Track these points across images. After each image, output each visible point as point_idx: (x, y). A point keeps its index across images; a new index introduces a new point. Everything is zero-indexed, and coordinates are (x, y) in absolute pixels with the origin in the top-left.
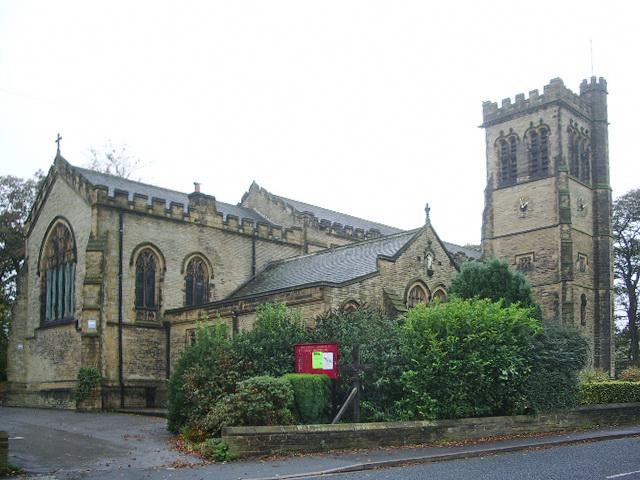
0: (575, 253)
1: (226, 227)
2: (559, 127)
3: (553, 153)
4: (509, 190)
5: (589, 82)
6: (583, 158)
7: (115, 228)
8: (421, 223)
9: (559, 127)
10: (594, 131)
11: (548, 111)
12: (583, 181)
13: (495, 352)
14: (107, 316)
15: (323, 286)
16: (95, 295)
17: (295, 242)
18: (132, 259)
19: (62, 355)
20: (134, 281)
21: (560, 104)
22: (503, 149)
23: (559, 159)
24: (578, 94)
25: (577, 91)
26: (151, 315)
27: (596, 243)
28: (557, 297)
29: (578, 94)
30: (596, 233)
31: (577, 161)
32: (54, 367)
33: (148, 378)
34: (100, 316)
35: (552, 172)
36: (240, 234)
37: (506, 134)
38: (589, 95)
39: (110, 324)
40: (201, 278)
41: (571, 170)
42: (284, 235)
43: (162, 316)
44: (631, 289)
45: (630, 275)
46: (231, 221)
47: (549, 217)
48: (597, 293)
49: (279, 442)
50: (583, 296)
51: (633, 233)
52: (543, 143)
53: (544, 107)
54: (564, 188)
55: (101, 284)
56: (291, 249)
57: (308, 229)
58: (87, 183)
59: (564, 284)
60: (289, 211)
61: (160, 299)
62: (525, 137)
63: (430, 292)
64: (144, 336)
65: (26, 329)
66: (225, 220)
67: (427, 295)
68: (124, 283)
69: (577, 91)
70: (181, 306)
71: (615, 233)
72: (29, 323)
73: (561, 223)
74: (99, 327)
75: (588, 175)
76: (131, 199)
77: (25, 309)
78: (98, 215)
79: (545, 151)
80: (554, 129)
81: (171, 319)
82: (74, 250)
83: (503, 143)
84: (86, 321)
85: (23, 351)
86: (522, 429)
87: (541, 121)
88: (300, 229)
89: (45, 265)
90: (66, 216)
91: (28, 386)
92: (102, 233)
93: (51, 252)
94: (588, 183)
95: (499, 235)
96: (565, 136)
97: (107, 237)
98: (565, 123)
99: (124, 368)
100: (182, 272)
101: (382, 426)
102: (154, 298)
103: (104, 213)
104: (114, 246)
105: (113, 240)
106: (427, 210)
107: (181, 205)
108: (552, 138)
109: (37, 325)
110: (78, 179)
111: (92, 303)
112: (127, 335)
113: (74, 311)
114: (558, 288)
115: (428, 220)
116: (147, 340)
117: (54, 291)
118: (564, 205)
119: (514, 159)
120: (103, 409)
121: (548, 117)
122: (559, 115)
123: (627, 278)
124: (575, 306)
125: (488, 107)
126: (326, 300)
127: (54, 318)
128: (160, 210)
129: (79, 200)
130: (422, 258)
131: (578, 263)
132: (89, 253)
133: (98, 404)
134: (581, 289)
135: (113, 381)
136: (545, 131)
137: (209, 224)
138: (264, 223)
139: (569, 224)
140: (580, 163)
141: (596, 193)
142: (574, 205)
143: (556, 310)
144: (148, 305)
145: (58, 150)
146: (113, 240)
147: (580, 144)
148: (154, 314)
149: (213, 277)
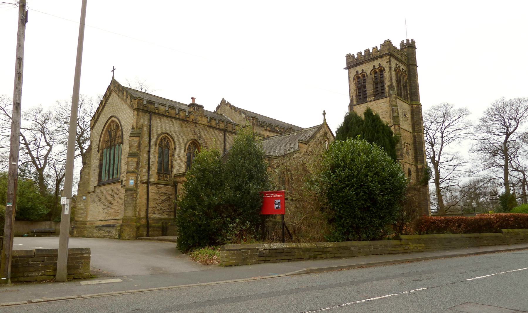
0: (403, 143)
1: (209, 124)
2: (390, 68)
3: (387, 83)
5: (405, 42)
6: (404, 87)
7: (147, 123)
8: (321, 122)
9: (390, 68)
10: (409, 71)
11: (384, 59)
12: (405, 99)
14: (141, 178)
16: (134, 164)
19: (111, 203)
20: (157, 155)
21: (391, 55)
23: (391, 87)
24: (399, 49)
25: (398, 47)
26: (166, 177)
27: (414, 137)
29: (399, 49)
30: (413, 133)
31: (401, 88)
32: (106, 210)
33: (164, 217)
34: (137, 177)
35: (387, 95)
37: (377, 67)
38: (405, 50)
39: (142, 182)
43: (173, 178)
50: (409, 169)
53: (381, 57)
60: (243, 116)
61: (172, 167)
62: (371, 74)
64: (162, 190)
65: (88, 186)
66: (209, 120)
68: (151, 157)
69: (398, 47)
72: (91, 183)
74: (136, 184)
75: (407, 96)
76: (156, 105)
77: (89, 174)
78: (138, 115)
79: (382, 82)
80: (387, 69)
83: (358, 78)
85: (86, 201)
87: (380, 65)
89: (102, 146)
91: (88, 223)
93: (107, 138)
94: (408, 101)
96: (394, 73)
98: (393, 66)
99: (150, 210)
100: (185, 151)
102: (168, 166)
103: (140, 114)
104: (146, 135)
106: (324, 114)
107: (184, 111)
108: (386, 74)
109: (96, 184)
110: (125, 93)
115: (325, 120)
116: (164, 193)
117: (108, 162)
118: (395, 114)
119: (365, 87)
121: (384, 62)
122: (390, 61)
127: (107, 179)
128: (172, 112)
129: (126, 106)
131: (405, 149)
134: (408, 165)
136: (382, 71)
138: (229, 122)
139: (399, 125)
140: (403, 89)
141: (412, 107)
142: (400, 114)
144: (165, 171)
145: (113, 77)
146: (146, 131)
148: (168, 176)
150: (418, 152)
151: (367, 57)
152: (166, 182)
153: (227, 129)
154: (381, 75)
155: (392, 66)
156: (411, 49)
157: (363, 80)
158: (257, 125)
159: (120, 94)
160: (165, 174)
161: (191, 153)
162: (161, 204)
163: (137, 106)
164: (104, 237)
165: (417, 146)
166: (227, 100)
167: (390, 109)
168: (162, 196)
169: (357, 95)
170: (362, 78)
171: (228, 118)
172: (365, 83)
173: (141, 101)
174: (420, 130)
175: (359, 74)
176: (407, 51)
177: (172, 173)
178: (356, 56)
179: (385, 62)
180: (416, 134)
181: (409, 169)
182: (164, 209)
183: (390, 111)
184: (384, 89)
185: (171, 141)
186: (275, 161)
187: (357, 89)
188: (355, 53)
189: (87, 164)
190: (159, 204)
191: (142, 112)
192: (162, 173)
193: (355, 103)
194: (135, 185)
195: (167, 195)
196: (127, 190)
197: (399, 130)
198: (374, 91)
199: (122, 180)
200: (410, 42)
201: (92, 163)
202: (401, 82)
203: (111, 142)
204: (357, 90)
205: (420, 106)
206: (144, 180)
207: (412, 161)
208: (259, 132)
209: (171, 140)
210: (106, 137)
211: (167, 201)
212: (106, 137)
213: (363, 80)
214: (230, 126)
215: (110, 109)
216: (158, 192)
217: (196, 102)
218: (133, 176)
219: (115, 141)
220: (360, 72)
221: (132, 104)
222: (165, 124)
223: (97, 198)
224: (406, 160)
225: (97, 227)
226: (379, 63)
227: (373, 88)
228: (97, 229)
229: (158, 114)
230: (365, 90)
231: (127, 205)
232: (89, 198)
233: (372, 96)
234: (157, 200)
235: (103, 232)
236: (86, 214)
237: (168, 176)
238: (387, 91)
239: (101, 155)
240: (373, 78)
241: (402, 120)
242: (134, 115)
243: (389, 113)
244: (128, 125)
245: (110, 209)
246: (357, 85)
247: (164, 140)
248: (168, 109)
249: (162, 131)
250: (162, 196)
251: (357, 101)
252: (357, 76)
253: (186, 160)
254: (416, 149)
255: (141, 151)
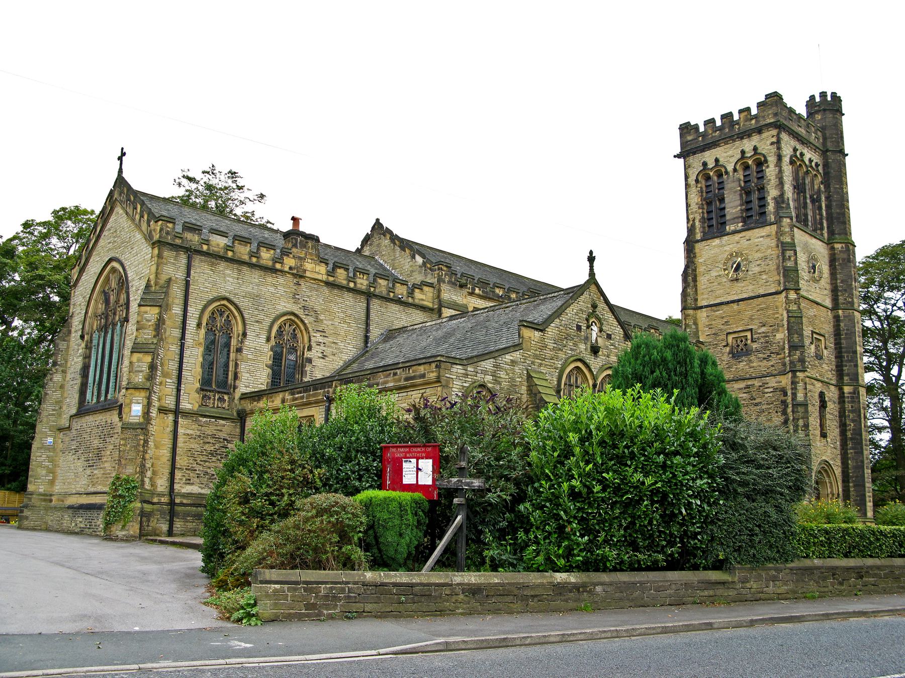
0: (807, 332)
1: (331, 279)
2: (780, 158)
3: (772, 193)
4: (717, 242)
7: (180, 275)
9: (780, 158)
11: (765, 135)
12: (815, 232)
13: (664, 466)
14: (159, 400)
15: (439, 362)
16: (145, 368)
17: (426, 303)
18: (200, 318)
20: (201, 349)
22: (707, 186)
23: (780, 200)
25: (802, 110)
26: (221, 400)
27: (837, 318)
28: (785, 394)
30: (836, 306)
31: (805, 204)
32: (88, 472)
34: (149, 398)
36: (350, 290)
37: (748, 155)
38: (818, 117)
39: (162, 410)
40: (294, 349)
41: (797, 217)
42: (411, 293)
43: (236, 401)
44: (891, 387)
45: (888, 369)
46: (339, 271)
47: (771, 282)
48: (841, 389)
49: (335, 598)
50: (822, 395)
51: (889, 307)
52: (758, 178)
53: (759, 131)
54: (788, 240)
55: (154, 354)
56: (418, 312)
57: (444, 287)
58: (150, 213)
59: (794, 376)
60: (419, 260)
61: (236, 377)
62: (735, 170)
63: (595, 378)
65: (60, 415)
67: (591, 382)
68: (187, 353)
69: (802, 110)
70: (264, 387)
71: (863, 306)
72: (64, 407)
73: (786, 289)
74: (146, 414)
75: (822, 224)
77: (62, 387)
78: (160, 256)
79: (762, 189)
80: (772, 159)
81: (248, 406)
82: (127, 304)
84: (130, 405)
85: (52, 448)
86: (711, 593)
87: (755, 149)
88: (431, 285)
90: (122, 259)
91: (54, 498)
92: (162, 282)
93: (101, 307)
94: (822, 234)
95: (705, 303)
96: (787, 170)
97: (168, 287)
98: (787, 152)
99: (178, 475)
100: (268, 339)
101: (495, 578)
102: (227, 374)
103: (166, 253)
105: (177, 291)
106: (591, 259)
108: (771, 171)
109: (74, 411)
110: (139, 207)
111: (140, 379)
112: (186, 427)
113: (119, 392)
114: (785, 381)
115: (592, 274)
116: (213, 436)
118: (789, 264)
119: (722, 200)
120: (141, 535)
121: (764, 143)
122: (778, 142)
123: (885, 372)
124: (810, 408)
125: (686, 129)
126: (444, 383)
127: (95, 400)
130: (584, 328)
131: (813, 347)
132: (143, 309)
133: (134, 528)
134: (819, 385)
135: (161, 495)
136: (761, 163)
137: (308, 274)
139: (797, 290)
140: (810, 206)
141: (833, 248)
143: (784, 413)
144: (218, 386)
145: (120, 171)
146: (177, 291)
147: (807, 181)
148: (226, 397)
149: (310, 348)
150: (845, 355)
151: (727, 130)
152: (220, 410)
153: (375, 290)
154: (758, 172)
155: (785, 153)
156: (831, 115)
157: (719, 183)
158: (450, 282)
159: (130, 211)
160: (219, 392)
161: (284, 345)
162: (205, 461)
163: (160, 237)
164: (80, 533)
165: (842, 341)
166: (386, 224)
167: (777, 252)
168: (209, 443)
169: (703, 218)
170: (715, 178)
171: (386, 265)
172: (721, 191)
173: (170, 225)
174: (849, 302)
175: (708, 169)
176: (821, 119)
177: (234, 391)
178: (702, 129)
179: (769, 142)
180: (840, 312)
181: (822, 395)
182: (213, 475)
183: (778, 257)
184: (764, 206)
185: (235, 317)
186: (454, 370)
187: (704, 203)
188: (698, 120)
189: (59, 365)
190: (201, 461)
191: (171, 250)
192: (213, 391)
193: (698, 236)
194: (143, 417)
195: (220, 442)
196: (126, 427)
197: (796, 302)
198: (741, 210)
199: (122, 404)
200: (829, 99)
201: (69, 365)
202: (807, 191)
203: (107, 318)
204: (705, 207)
205: (851, 247)
206: (167, 405)
207: (830, 376)
208: (454, 298)
209: (236, 314)
210: (100, 306)
211: (220, 455)
212: (100, 306)
213: (719, 183)
214: (383, 284)
215: (109, 243)
216: (198, 433)
217: (302, 228)
218: (141, 396)
219: (115, 314)
220: (711, 165)
221: (151, 231)
222: (225, 277)
223: (74, 442)
224: (811, 372)
225: (70, 507)
226: (755, 146)
227: (739, 202)
228: (70, 511)
229: (207, 254)
230: (723, 206)
231: (123, 462)
232: (60, 441)
233: (736, 220)
234: (196, 453)
235: (81, 520)
236: (51, 478)
237: (226, 397)
238: (772, 210)
239: (86, 346)
240: (739, 180)
241: (806, 278)
242: (152, 257)
243: (775, 261)
244: (140, 279)
245: (96, 469)
246: (704, 194)
247: (221, 315)
248: (233, 243)
249: (215, 295)
250: (209, 443)
251: (704, 232)
252: (705, 174)
253: (271, 362)
254: (841, 348)
255: (162, 339)
